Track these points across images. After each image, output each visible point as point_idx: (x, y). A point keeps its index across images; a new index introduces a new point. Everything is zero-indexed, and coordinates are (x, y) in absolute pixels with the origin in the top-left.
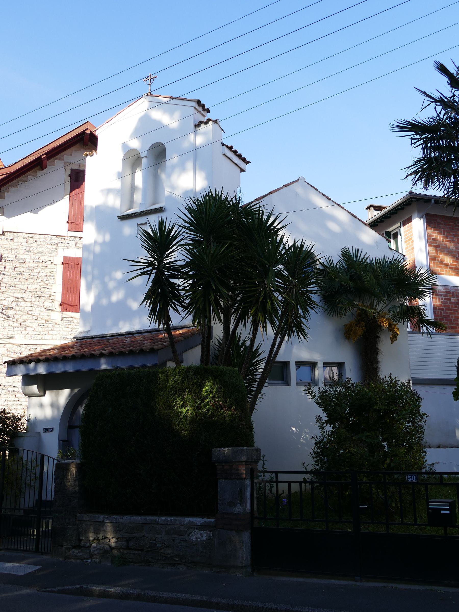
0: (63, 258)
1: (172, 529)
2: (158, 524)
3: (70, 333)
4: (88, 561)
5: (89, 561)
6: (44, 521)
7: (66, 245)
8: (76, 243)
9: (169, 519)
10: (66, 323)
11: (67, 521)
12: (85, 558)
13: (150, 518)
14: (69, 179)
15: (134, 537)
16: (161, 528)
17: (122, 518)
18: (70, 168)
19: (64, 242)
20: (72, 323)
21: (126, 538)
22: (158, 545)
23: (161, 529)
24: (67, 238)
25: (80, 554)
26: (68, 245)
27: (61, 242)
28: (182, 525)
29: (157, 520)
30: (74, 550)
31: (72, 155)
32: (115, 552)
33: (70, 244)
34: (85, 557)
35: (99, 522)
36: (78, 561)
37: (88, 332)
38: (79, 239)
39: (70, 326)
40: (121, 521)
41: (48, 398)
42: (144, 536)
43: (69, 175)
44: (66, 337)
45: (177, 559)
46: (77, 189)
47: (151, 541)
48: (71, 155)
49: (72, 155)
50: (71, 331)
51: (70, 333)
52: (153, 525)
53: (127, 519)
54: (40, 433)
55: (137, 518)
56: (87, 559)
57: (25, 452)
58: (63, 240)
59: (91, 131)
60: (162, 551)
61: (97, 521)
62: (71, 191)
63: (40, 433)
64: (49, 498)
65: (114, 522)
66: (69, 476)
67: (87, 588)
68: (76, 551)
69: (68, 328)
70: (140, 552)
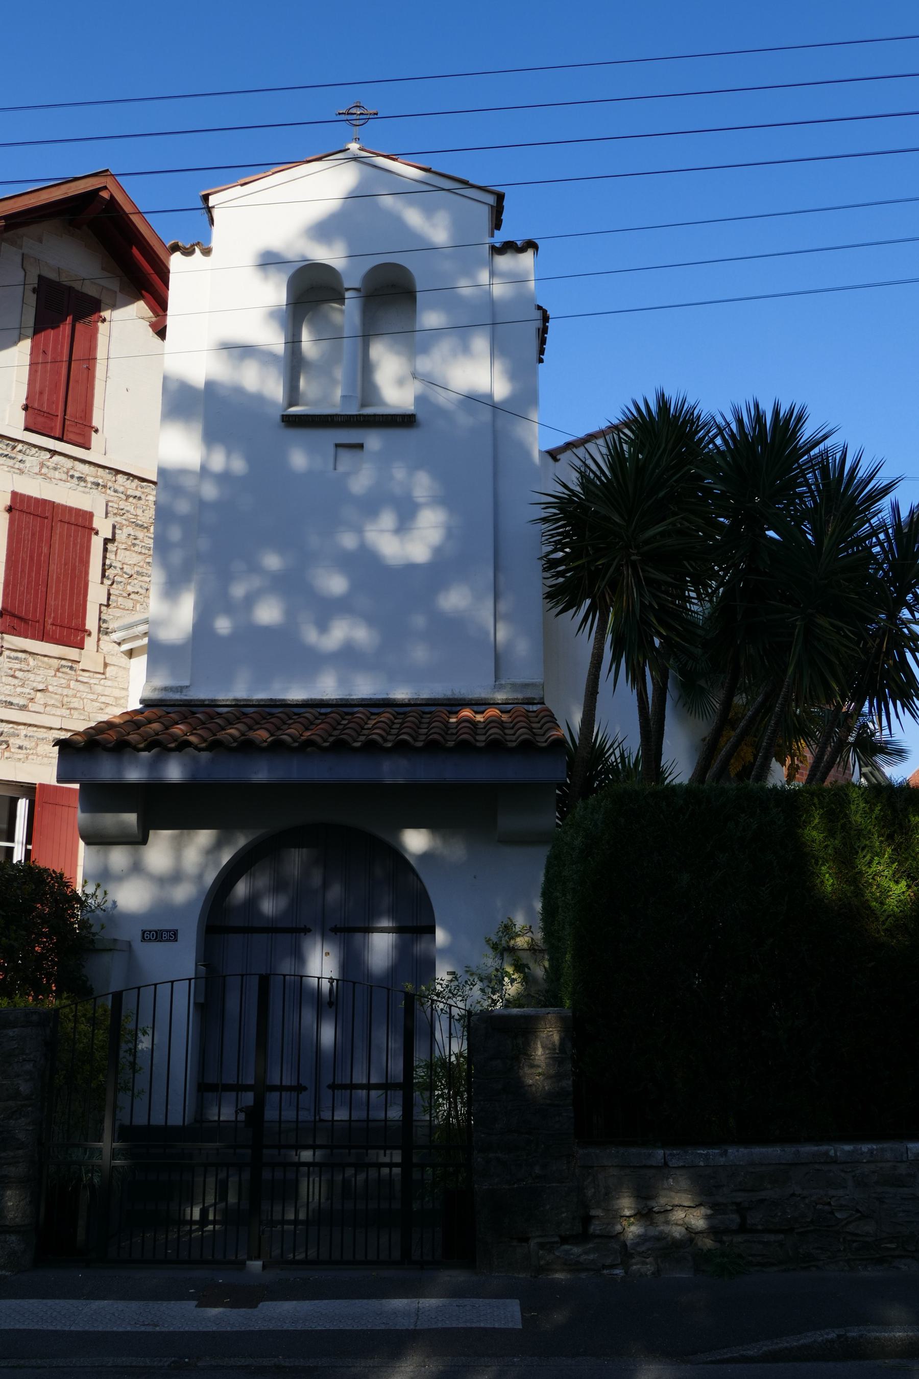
0: (9, 496)
1: (873, 1172)
2: (834, 1161)
3: (19, 690)
4: (617, 1271)
5: (619, 1272)
6: (211, 1181)
7: (18, 465)
8: (42, 465)
9: (865, 1148)
10: (11, 665)
11: (537, 1170)
12: (604, 1267)
13: (808, 1149)
14: (32, 299)
15: (762, 1201)
16: (842, 1171)
17: (725, 1153)
18: (38, 272)
19: (13, 455)
20: (23, 666)
21: (738, 1204)
22: (838, 1215)
23: (843, 1174)
24: (20, 447)
25: (591, 1257)
26: (22, 466)
27: (6, 453)
28: (902, 1162)
29: (832, 1153)
30: (567, 1247)
31: (41, 242)
32: (708, 1243)
33: (28, 464)
34: (608, 1262)
35: (651, 1167)
36: (583, 1275)
37: (180, 689)
38: (49, 455)
39: (19, 674)
40: (722, 1160)
41: (160, 852)
42: (793, 1195)
43: (34, 290)
44: (8, 699)
45: (893, 1246)
46: (53, 328)
47: (819, 1207)
48: (40, 241)
49: (41, 242)
50: (22, 686)
51: (19, 690)
52: (817, 1166)
53: (737, 1154)
54: (129, 944)
55: (770, 1150)
56: (612, 1266)
57: (147, 993)
58: (9, 449)
59: (112, 196)
60: (851, 1228)
61: (645, 1167)
62: (36, 332)
63: (129, 944)
64: (176, 1119)
65: (702, 1164)
66: (535, 1049)
67: (861, 1336)
68: (576, 1250)
69: (13, 676)
70: (781, 1236)
